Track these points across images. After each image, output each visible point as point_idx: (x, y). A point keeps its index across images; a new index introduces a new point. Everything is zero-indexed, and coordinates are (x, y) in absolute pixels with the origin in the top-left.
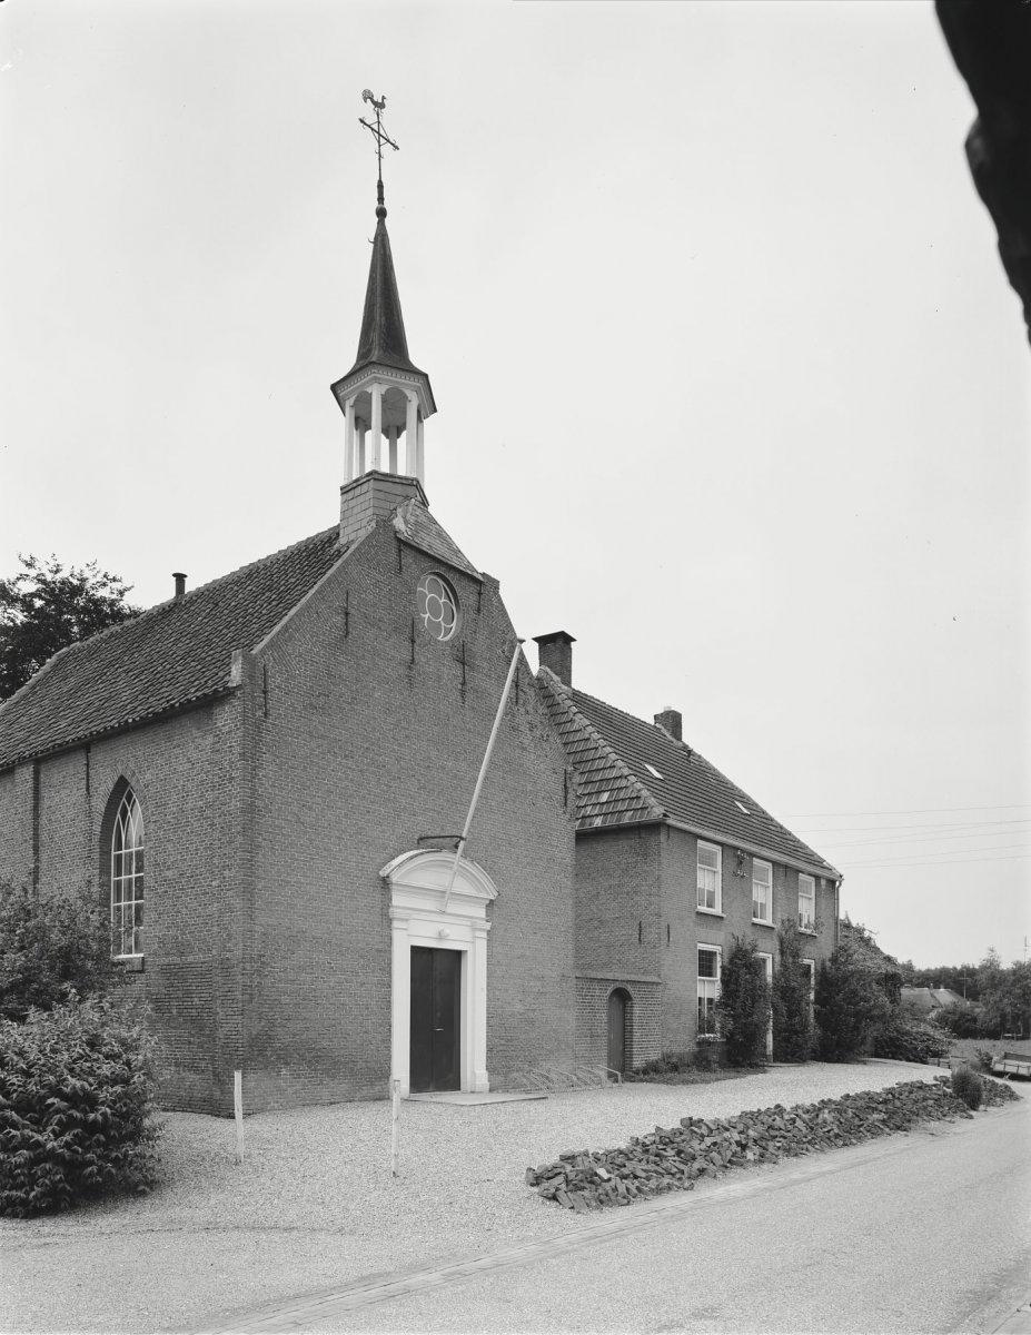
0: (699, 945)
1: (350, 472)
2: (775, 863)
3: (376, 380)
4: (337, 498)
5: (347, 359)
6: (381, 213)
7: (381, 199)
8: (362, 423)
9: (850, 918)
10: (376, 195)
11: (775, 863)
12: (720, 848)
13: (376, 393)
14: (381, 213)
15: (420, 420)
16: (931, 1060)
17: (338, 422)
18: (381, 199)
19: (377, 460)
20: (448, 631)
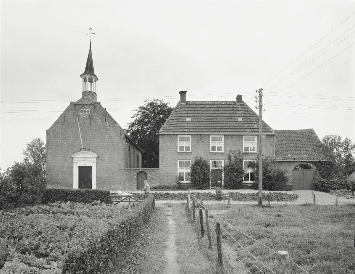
0: (223, 161)
1: (83, 90)
2: (224, 135)
3: (87, 76)
4: (81, 94)
5: (83, 70)
6: (90, 47)
7: (91, 45)
8: (85, 80)
9: (128, 122)
10: (90, 44)
11: (224, 135)
12: (223, 136)
13: (87, 78)
14: (90, 47)
15: (95, 81)
16: (332, 191)
17: (81, 80)
18: (91, 45)
19: (88, 89)
20: (82, 115)
